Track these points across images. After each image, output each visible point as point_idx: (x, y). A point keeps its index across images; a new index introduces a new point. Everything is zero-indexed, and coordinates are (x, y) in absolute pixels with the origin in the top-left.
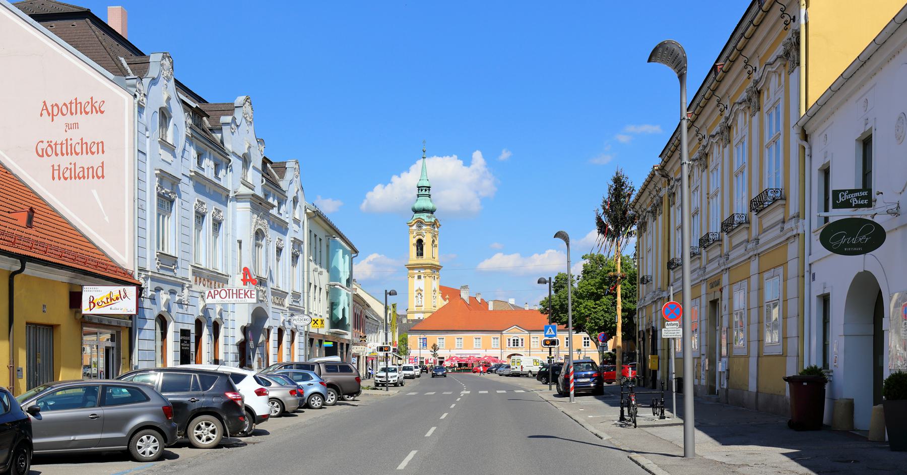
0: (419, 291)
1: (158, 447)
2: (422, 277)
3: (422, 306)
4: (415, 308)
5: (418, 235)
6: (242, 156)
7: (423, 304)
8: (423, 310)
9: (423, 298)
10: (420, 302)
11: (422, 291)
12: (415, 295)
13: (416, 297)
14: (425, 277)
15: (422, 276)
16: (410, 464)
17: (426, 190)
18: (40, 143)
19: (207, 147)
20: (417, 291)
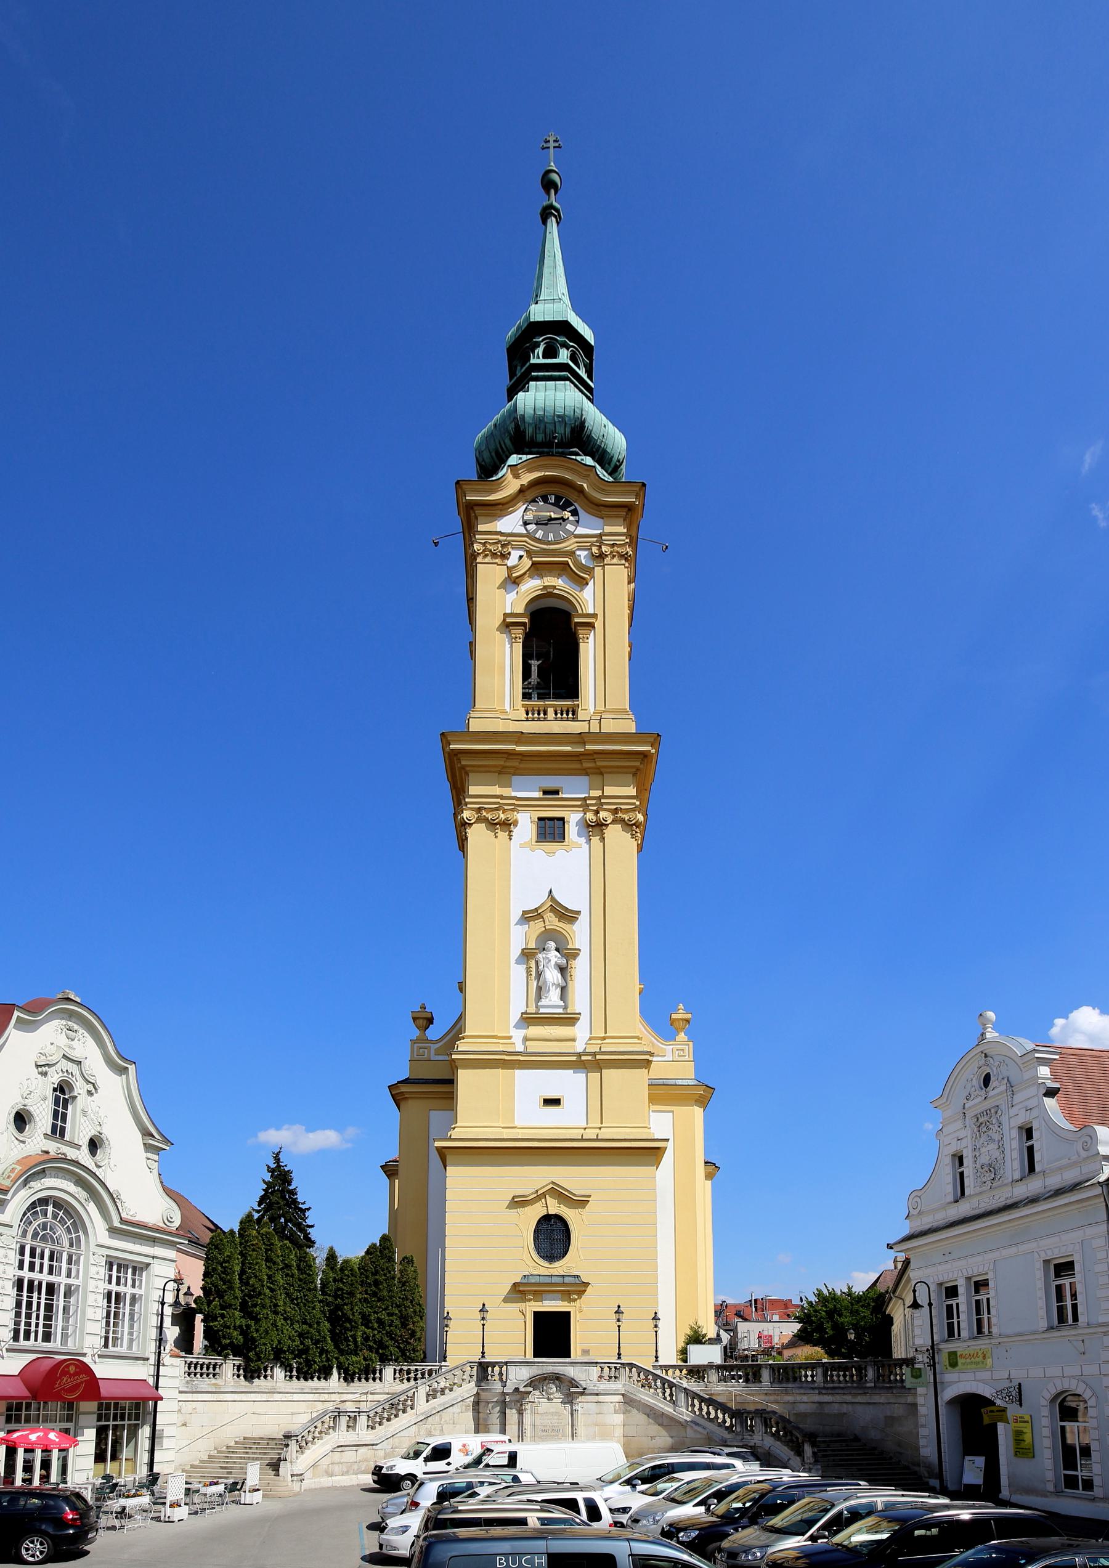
0: (552, 921)
1: (45, 1553)
2: (572, 830)
3: (570, 1020)
4: (518, 1035)
5: (537, 569)
6: (40, 1153)
7: (579, 1002)
8: (579, 1047)
9: (580, 967)
10: (553, 997)
11: (569, 916)
12: (519, 937)
13: (527, 955)
14: (599, 826)
15: (573, 819)
16: (541, 375)
17: (531, 974)
18: (173, 1282)
19: (931, 1292)
20: (528, 917)
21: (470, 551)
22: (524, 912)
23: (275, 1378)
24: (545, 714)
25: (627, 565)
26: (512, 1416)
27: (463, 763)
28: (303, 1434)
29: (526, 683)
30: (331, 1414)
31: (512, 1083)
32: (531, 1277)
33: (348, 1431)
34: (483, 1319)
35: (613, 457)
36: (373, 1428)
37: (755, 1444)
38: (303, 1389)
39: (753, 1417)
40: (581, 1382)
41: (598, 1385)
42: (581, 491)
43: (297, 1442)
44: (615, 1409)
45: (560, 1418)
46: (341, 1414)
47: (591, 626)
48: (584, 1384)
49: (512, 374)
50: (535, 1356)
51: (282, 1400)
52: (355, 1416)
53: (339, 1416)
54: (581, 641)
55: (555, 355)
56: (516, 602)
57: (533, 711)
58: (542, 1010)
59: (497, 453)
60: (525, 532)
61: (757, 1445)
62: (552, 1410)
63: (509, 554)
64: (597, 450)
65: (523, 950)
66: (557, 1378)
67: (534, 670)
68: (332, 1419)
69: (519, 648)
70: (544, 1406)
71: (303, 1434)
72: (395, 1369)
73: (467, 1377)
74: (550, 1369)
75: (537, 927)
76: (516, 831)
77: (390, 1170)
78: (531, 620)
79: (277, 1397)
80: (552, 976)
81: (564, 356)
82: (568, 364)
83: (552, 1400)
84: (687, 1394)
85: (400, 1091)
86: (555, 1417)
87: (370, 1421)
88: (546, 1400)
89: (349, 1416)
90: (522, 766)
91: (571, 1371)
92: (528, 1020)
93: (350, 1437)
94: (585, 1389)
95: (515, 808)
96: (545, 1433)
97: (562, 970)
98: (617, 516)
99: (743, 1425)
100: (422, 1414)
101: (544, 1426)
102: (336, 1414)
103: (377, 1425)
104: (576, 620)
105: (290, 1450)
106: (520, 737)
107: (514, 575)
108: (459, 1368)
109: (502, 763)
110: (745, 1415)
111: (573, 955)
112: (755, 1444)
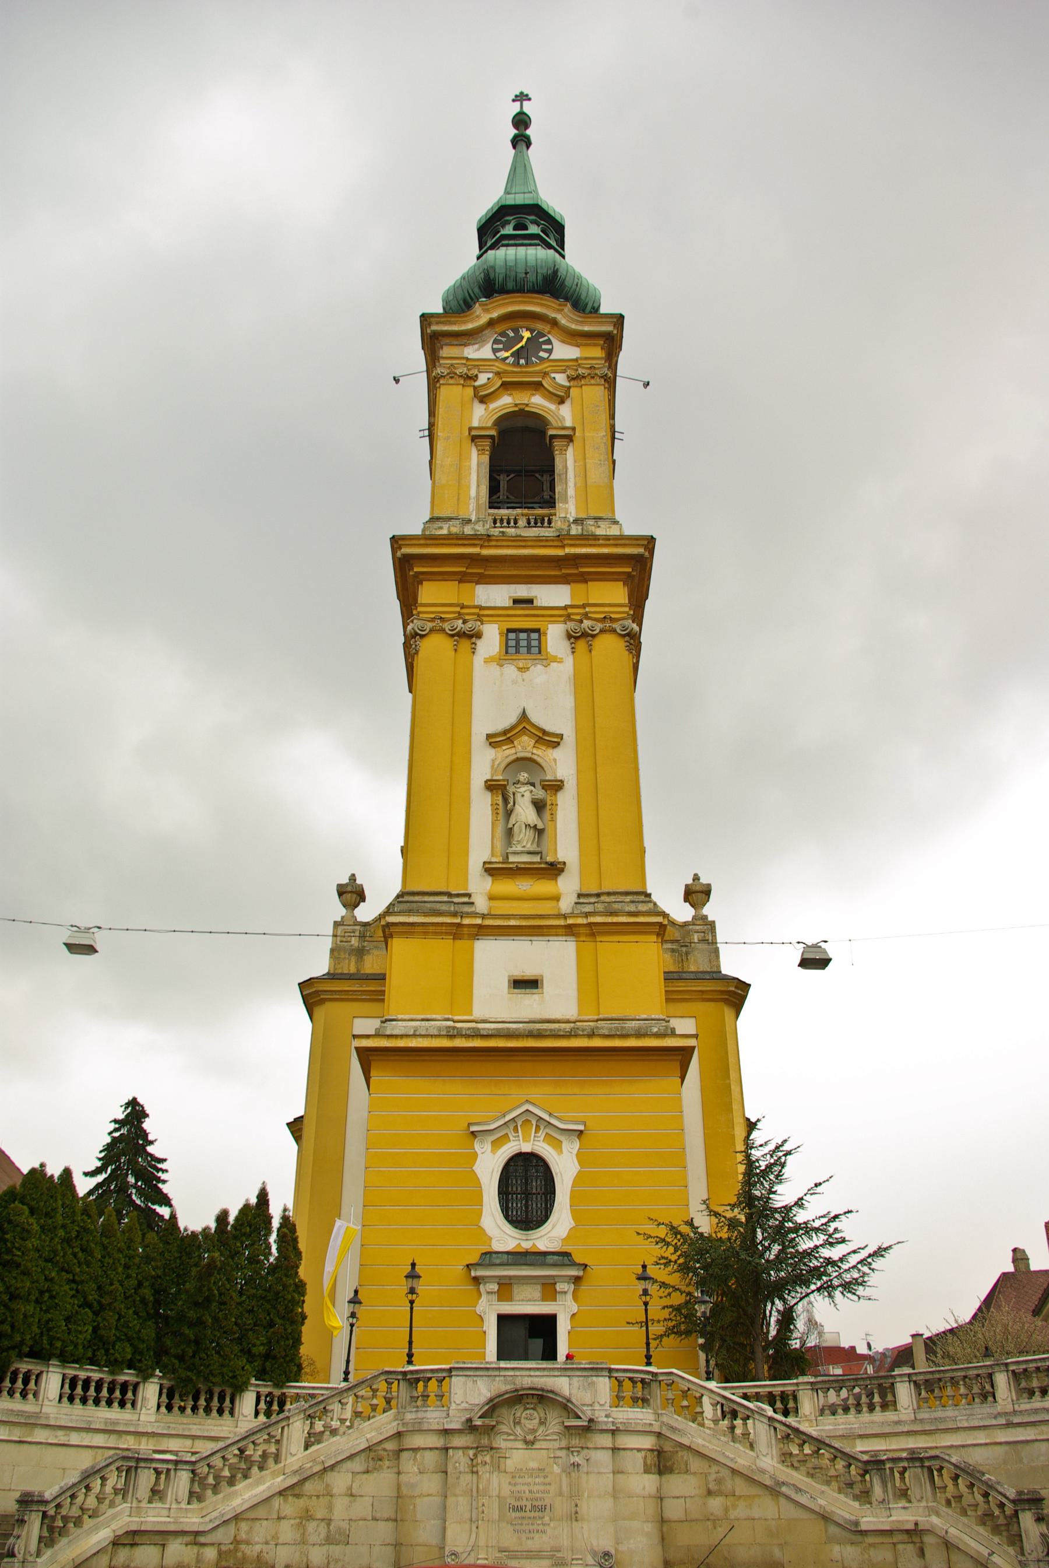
5: (506, 386)
8: (566, 904)
9: (566, 806)
10: (524, 840)
11: (549, 740)
20: (494, 740)
21: (434, 374)
22: (489, 736)
23: (41, 1398)
24: (516, 523)
25: (607, 386)
26: (458, 1478)
27: (416, 569)
28: (59, 1500)
29: (494, 497)
30: (119, 1463)
31: (473, 948)
32: (494, 1255)
33: (150, 1502)
34: (412, 1291)
35: (586, 305)
36: (200, 1498)
37: (916, 1524)
38: (90, 1422)
39: (905, 1469)
40: (585, 1408)
41: (614, 1415)
42: (554, 323)
43: (45, 1514)
44: (645, 1464)
45: (547, 1480)
46: (142, 1464)
47: (570, 439)
48: (587, 1413)
49: (481, 248)
50: (501, 1356)
51: (50, 1441)
52: (168, 1470)
53: (136, 1468)
54: (557, 452)
55: (526, 228)
56: (481, 416)
57: (502, 520)
58: (512, 859)
59: (465, 301)
60: (494, 357)
61: (920, 1527)
62: (533, 1465)
63: (476, 376)
64: (572, 296)
65: (486, 782)
66: (542, 1398)
67: (503, 485)
68: (124, 1474)
69: (486, 458)
70: (517, 1457)
71: (59, 1500)
72: (258, 1392)
73: (379, 1401)
74: (526, 1381)
75: (507, 753)
76: (481, 644)
77: (296, 1127)
78: (501, 433)
79: (41, 1435)
80: (525, 813)
81: (533, 229)
82: (539, 235)
83: (533, 1443)
84: (775, 1429)
85: (314, 990)
86: (537, 1480)
87: (196, 1483)
88: (520, 1445)
89: (155, 1469)
90: (486, 573)
91: (563, 1385)
92: (491, 870)
93: (155, 1517)
94: (591, 1420)
95: (480, 618)
96: (518, 1514)
97: (539, 806)
98: (595, 345)
99: (886, 1486)
100: (295, 1472)
101: (518, 1499)
102: (133, 1464)
103: (209, 1492)
104: (551, 432)
105: (24, 1533)
106: (486, 539)
107: (481, 394)
108: (367, 1383)
109: (463, 569)
110: (888, 1465)
111: (557, 786)
112: (916, 1524)
